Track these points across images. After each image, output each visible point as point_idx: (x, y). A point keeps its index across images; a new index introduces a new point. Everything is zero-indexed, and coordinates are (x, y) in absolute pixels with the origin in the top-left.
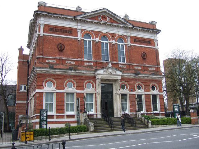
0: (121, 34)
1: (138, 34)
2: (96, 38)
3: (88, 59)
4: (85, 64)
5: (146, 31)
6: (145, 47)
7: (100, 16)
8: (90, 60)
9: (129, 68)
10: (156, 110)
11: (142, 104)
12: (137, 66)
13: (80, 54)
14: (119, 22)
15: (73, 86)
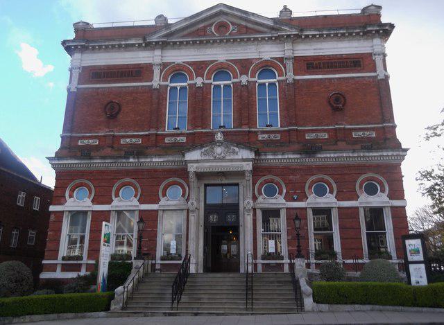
0: (266, 57)
1: (313, 47)
2: (241, 74)
3: (267, 126)
4: (167, 140)
5: (343, 35)
6: (340, 79)
7: (211, 25)
8: (273, 128)
9: (287, 140)
11: (385, 233)
12: (313, 131)
13: (156, 118)
14: (261, 29)
15: (379, 190)
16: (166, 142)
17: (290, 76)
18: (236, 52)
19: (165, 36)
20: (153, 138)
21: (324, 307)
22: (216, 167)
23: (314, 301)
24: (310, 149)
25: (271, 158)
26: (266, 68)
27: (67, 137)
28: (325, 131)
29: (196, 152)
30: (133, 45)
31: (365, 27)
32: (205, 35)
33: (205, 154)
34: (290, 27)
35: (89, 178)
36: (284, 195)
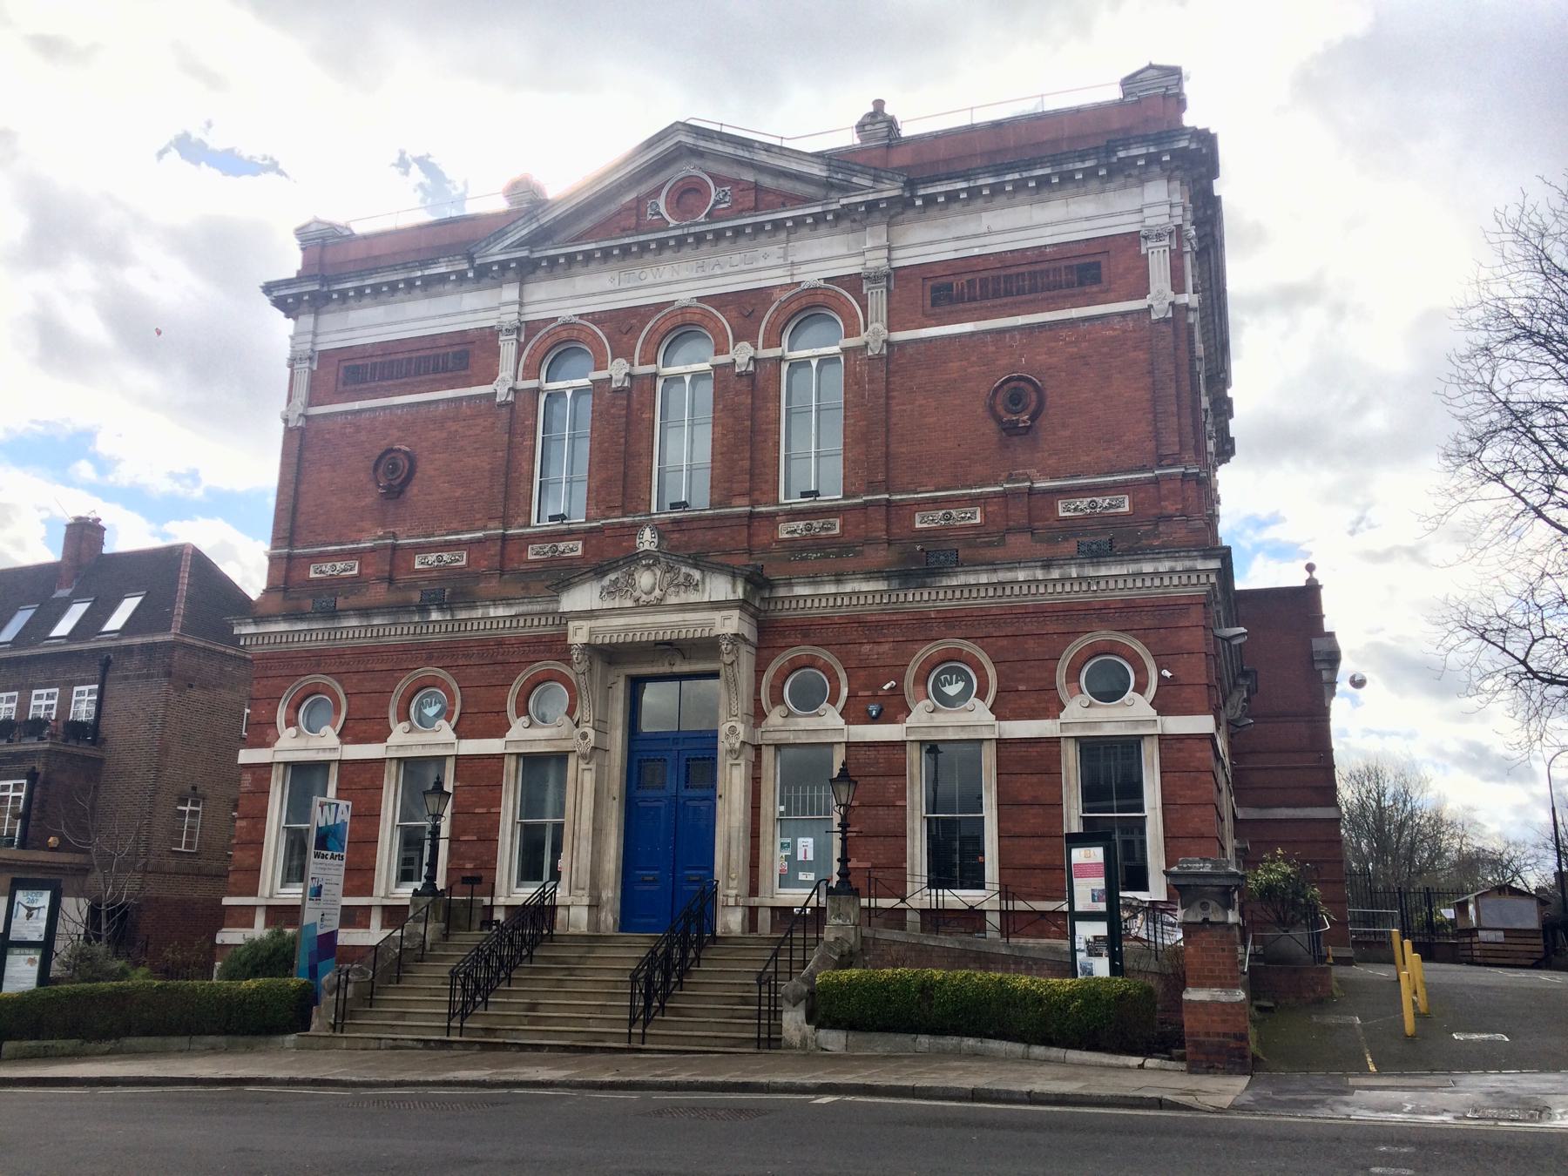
0: (811, 276)
2: (737, 339)
5: (1043, 182)
6: (1030, 328)
7: (657, 192)
10: (1144, 887)
12: (936, 503)
13: (509, 485)
16: (530, 557)
17: (875, 334)
18: (728, 269)
19: (855, 189)
20: (495, 549)
21: (834, 1040)
22: (643, 627)
23: (809, 1020)
24: (922, 562)
25: (807, 595)
26: (809, 307)
27: (280, 557)
28: (974, 500)
29: (587, 587)
30: (443, 278)
31: (1110, 149)
32: (638, 230)
33: (610, 592)
34: (897, 172)
35: (334, 669)
36: (841, 704)
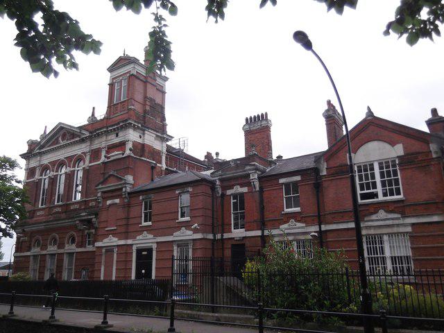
26: (79, 159)
